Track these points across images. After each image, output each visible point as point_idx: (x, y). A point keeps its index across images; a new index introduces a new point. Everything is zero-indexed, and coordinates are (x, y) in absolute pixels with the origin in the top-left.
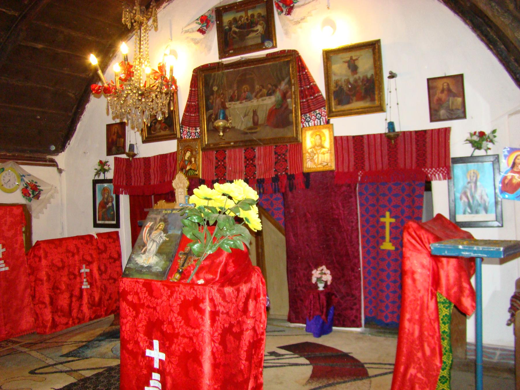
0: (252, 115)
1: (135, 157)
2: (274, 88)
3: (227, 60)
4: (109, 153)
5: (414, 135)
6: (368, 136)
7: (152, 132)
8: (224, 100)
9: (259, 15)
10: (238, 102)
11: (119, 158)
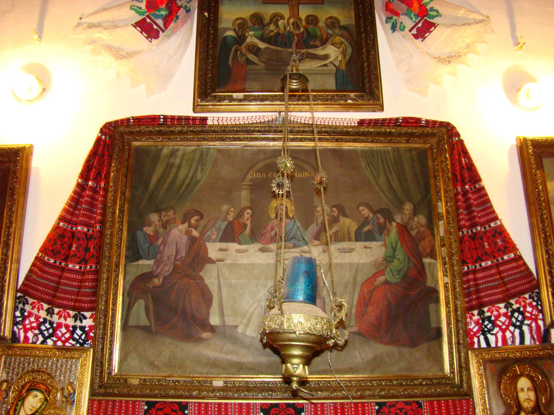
8: (202, 234)
9: (333, 23)
10: (258, 246)
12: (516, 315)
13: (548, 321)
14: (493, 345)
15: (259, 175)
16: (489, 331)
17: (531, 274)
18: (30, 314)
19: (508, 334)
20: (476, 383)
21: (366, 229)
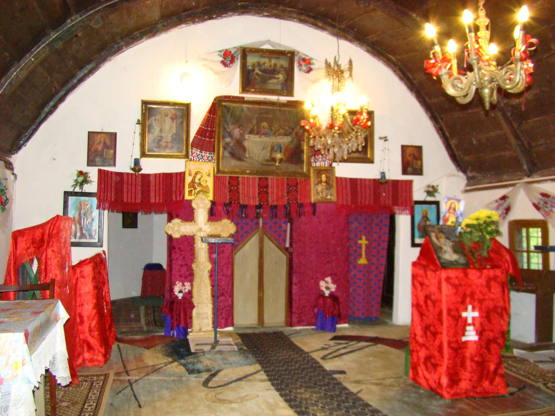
0: (270, 149)
2: (291, 130)
3: (249, 96)
4: (91, 162)
6: (361, 179)
8: (244, 132)
9: (282, 66)
11: (105, 171)
18: (194, 153)
20: (312, 175)
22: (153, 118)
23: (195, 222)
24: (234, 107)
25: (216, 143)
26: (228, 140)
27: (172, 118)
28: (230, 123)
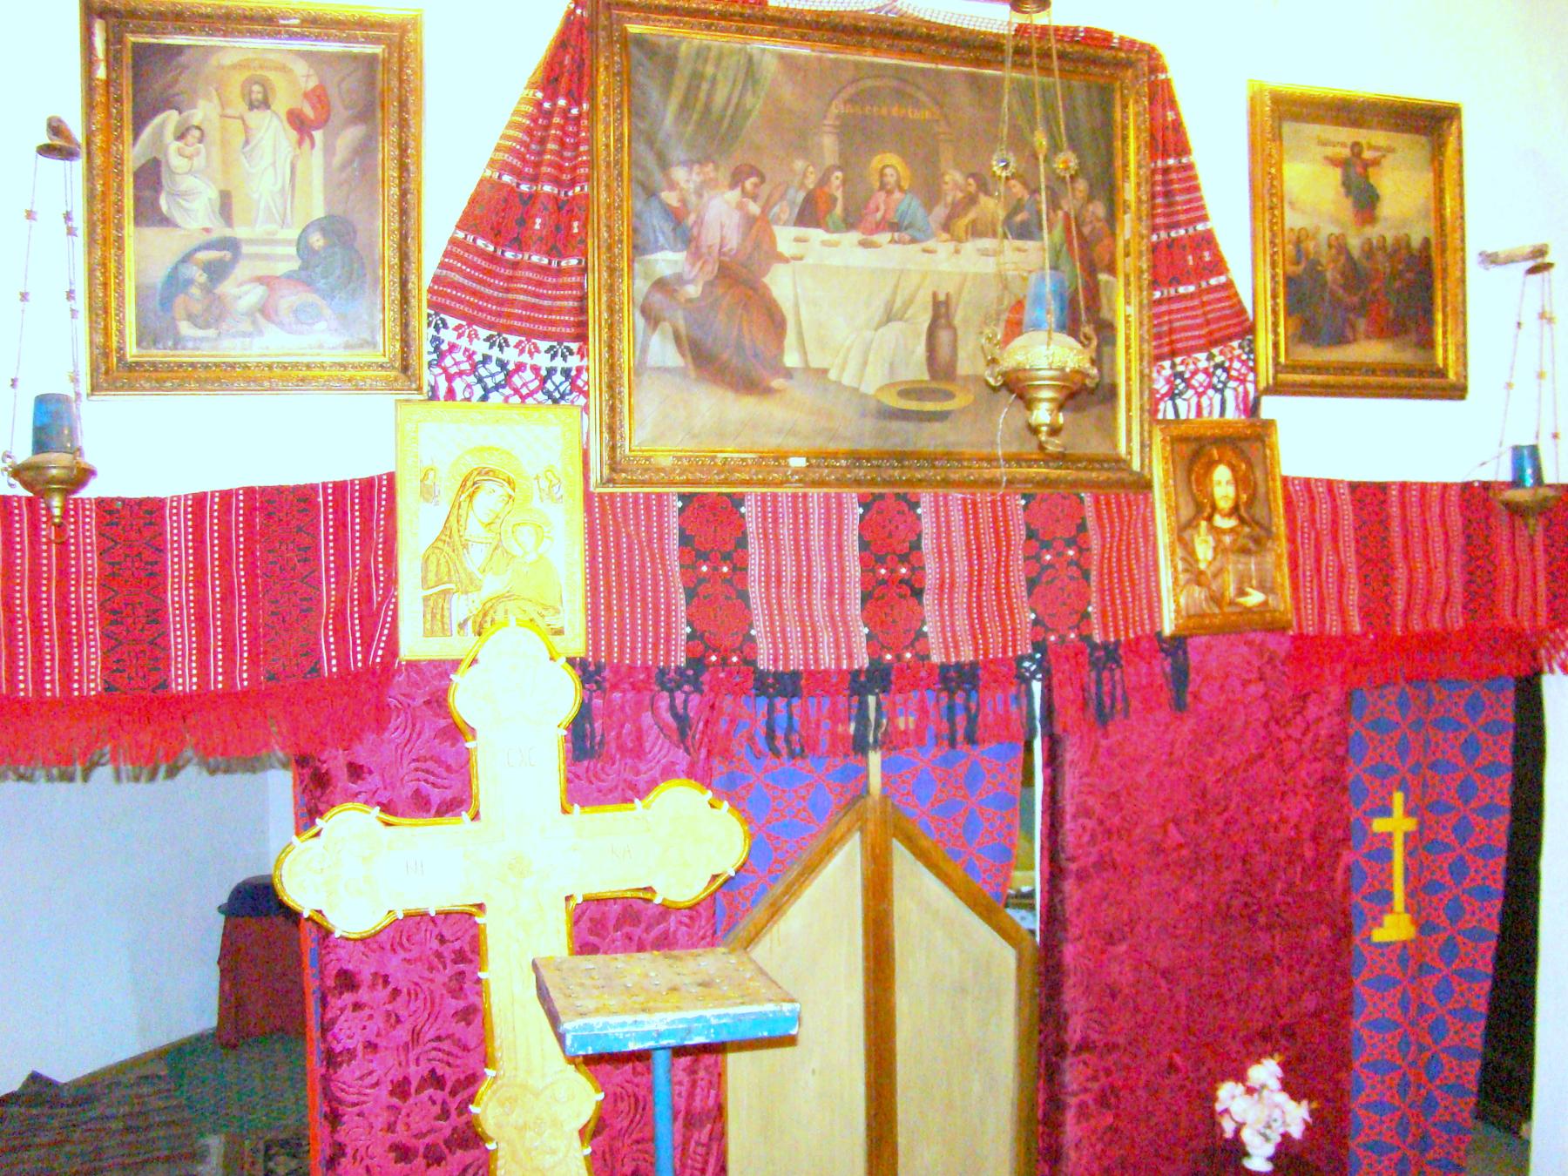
0: (925, 320)
1: (84, 493)
5: (1453, 497)
7: (185, 328)
10: (855, 236)
12: (1219, 372)
13: (1262, 384)
14: (1183, 416)
15: (849, 110)
16: (1181, 394)
17: (1242, 311)
18: (452, 347)
19: (1205, 401)
21: (1019, 218)
22: (170, 119)
23: (476, 817)
24: (702, 54)
25: (592, 283)
26: (667, 261)
27: (300, 124)
28: (677, 153)
